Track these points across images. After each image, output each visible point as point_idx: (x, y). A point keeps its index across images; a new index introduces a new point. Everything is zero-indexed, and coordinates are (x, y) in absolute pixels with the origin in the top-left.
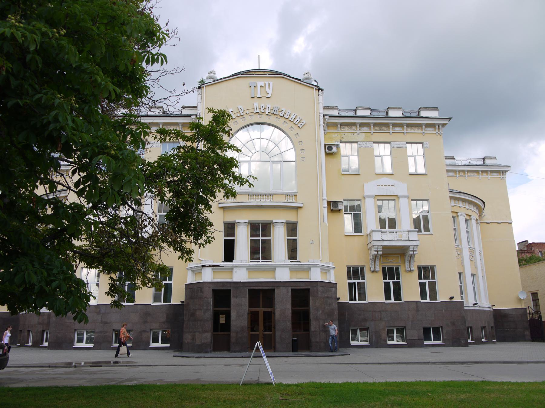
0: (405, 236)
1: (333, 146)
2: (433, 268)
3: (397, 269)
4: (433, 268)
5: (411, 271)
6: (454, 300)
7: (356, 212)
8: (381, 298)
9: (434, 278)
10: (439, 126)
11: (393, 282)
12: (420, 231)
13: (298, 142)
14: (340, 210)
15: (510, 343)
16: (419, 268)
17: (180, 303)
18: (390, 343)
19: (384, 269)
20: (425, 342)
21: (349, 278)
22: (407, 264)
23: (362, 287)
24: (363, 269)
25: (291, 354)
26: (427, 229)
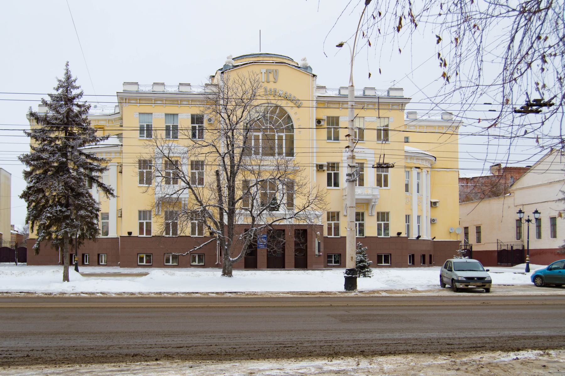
0: (370, 192)
1: (321, 121)
2: (388, 213)
3: (363, 214)
4: (388, 213)
5: (372, 215)
6: (132, 235)
7: (336, 172)
8: (375, 234)
9: (388, 220)
10: (402, 105)
11: (334, 223)
12: (381, 186)
13: (140, 113)
14: (324, 170)
15: (32, 266)
16: (378, 213)
17: (127, 235)
18: (194, 264)
19: (166, 212)
20: (329, 264)
21: (140, 219)
22: (370, 211)
23: (149, 225)
24: (338, 213)
25: (324, 269)
26: (386, 185)
